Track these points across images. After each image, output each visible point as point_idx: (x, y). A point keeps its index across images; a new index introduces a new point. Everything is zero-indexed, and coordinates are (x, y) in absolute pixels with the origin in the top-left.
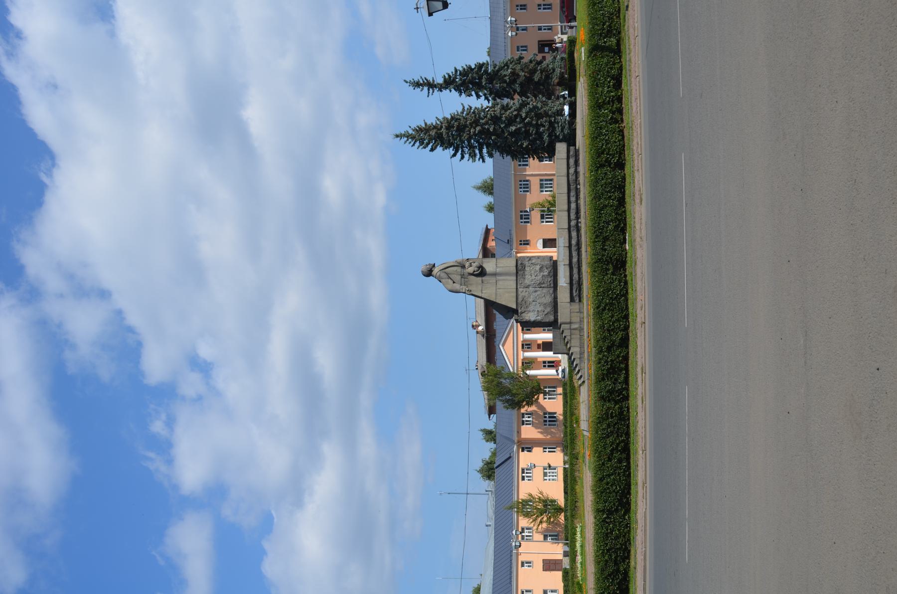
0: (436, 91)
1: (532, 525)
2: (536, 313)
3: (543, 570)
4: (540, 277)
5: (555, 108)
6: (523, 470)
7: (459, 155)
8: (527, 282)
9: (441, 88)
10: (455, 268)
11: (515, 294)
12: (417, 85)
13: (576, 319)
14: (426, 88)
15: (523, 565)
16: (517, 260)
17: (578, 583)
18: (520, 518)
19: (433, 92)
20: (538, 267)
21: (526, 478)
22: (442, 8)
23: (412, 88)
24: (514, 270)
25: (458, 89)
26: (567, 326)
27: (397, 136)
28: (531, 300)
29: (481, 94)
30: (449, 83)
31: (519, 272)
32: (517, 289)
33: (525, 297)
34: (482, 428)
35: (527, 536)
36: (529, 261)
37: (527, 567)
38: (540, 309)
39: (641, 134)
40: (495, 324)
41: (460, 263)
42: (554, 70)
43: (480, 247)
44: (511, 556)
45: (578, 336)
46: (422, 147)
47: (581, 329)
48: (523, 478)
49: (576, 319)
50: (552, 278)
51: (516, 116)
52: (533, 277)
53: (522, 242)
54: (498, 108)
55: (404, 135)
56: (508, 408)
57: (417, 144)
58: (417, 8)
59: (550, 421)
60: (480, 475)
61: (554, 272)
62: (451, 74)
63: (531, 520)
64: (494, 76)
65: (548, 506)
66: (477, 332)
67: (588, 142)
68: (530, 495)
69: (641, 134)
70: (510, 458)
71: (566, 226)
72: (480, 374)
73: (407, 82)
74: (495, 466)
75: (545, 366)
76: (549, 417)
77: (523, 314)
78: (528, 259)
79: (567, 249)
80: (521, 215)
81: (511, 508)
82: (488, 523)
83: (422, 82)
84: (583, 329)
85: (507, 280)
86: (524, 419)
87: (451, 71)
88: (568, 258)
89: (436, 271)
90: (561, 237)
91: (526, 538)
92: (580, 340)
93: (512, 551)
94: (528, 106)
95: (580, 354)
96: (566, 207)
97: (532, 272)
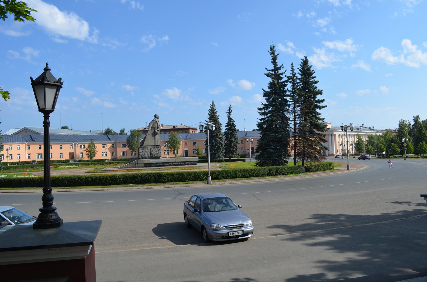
0: (228, 115)
1: (86, 148)
2: (142, 152)
4: (154, 153)
5: (220, 155)
6: (106, 145)
8: (152, 149)
9: (229, 117)
10: (157, 125)
11: (148, 145)
12: (230, 109)
13: (139, 165)
14: (229, 112)
16: (159, 146)
17: (58, 167)
18: (88, 144)
19: (227, 114)
20: (157, 152)
21: (103, 146)
23: (229, 107)
24: (157, 145)
25: (228, 122)
27: (213, 102)
28: (146, 150)
29: (227, 130)
30: (230, 120)
31: (156, 146)
32: (150, 146)
33: (147, 148)
34: (125, 129)
35: (82, 147)
38: (143, 153)
39: (279, 180)
41: (159, 127)
42: (234, 155)
43: (189, 127)
46: (209, 110)
48: (103, 145)
49: (139, 165)
51: (218, 142)
52: (154, 151)
54: (220, 136)
55: (213, 104)
56: (127, 139)
57: (210, 109)
58: (201, 122)
59: (123, 154)
60: (106, 129)
62: (233, 120)
63: (87, 148)
64: (232, 135)
65: (92, 154)
68: (96, 148)
69: (279, 180)
70: (110, 140)
71: (170, 162)
72: (145, 127)
73: (230, 105)
74: (108, 135)
76: (125, 154)
77: (141, 148)
78: (160, 149)
79: (162, 162)
80: (196, 142)
81: (91, 141)
82: (91, 131)
83: (231, 110)
84: (135, 168)
86: (82, 145)
87: (234, 120)
88: (159, 162)
89: (156, 119)
91: (81, 146)
94: (221, 146)
95: (127, 167)
96: (177, 161)
97: (156, 151)
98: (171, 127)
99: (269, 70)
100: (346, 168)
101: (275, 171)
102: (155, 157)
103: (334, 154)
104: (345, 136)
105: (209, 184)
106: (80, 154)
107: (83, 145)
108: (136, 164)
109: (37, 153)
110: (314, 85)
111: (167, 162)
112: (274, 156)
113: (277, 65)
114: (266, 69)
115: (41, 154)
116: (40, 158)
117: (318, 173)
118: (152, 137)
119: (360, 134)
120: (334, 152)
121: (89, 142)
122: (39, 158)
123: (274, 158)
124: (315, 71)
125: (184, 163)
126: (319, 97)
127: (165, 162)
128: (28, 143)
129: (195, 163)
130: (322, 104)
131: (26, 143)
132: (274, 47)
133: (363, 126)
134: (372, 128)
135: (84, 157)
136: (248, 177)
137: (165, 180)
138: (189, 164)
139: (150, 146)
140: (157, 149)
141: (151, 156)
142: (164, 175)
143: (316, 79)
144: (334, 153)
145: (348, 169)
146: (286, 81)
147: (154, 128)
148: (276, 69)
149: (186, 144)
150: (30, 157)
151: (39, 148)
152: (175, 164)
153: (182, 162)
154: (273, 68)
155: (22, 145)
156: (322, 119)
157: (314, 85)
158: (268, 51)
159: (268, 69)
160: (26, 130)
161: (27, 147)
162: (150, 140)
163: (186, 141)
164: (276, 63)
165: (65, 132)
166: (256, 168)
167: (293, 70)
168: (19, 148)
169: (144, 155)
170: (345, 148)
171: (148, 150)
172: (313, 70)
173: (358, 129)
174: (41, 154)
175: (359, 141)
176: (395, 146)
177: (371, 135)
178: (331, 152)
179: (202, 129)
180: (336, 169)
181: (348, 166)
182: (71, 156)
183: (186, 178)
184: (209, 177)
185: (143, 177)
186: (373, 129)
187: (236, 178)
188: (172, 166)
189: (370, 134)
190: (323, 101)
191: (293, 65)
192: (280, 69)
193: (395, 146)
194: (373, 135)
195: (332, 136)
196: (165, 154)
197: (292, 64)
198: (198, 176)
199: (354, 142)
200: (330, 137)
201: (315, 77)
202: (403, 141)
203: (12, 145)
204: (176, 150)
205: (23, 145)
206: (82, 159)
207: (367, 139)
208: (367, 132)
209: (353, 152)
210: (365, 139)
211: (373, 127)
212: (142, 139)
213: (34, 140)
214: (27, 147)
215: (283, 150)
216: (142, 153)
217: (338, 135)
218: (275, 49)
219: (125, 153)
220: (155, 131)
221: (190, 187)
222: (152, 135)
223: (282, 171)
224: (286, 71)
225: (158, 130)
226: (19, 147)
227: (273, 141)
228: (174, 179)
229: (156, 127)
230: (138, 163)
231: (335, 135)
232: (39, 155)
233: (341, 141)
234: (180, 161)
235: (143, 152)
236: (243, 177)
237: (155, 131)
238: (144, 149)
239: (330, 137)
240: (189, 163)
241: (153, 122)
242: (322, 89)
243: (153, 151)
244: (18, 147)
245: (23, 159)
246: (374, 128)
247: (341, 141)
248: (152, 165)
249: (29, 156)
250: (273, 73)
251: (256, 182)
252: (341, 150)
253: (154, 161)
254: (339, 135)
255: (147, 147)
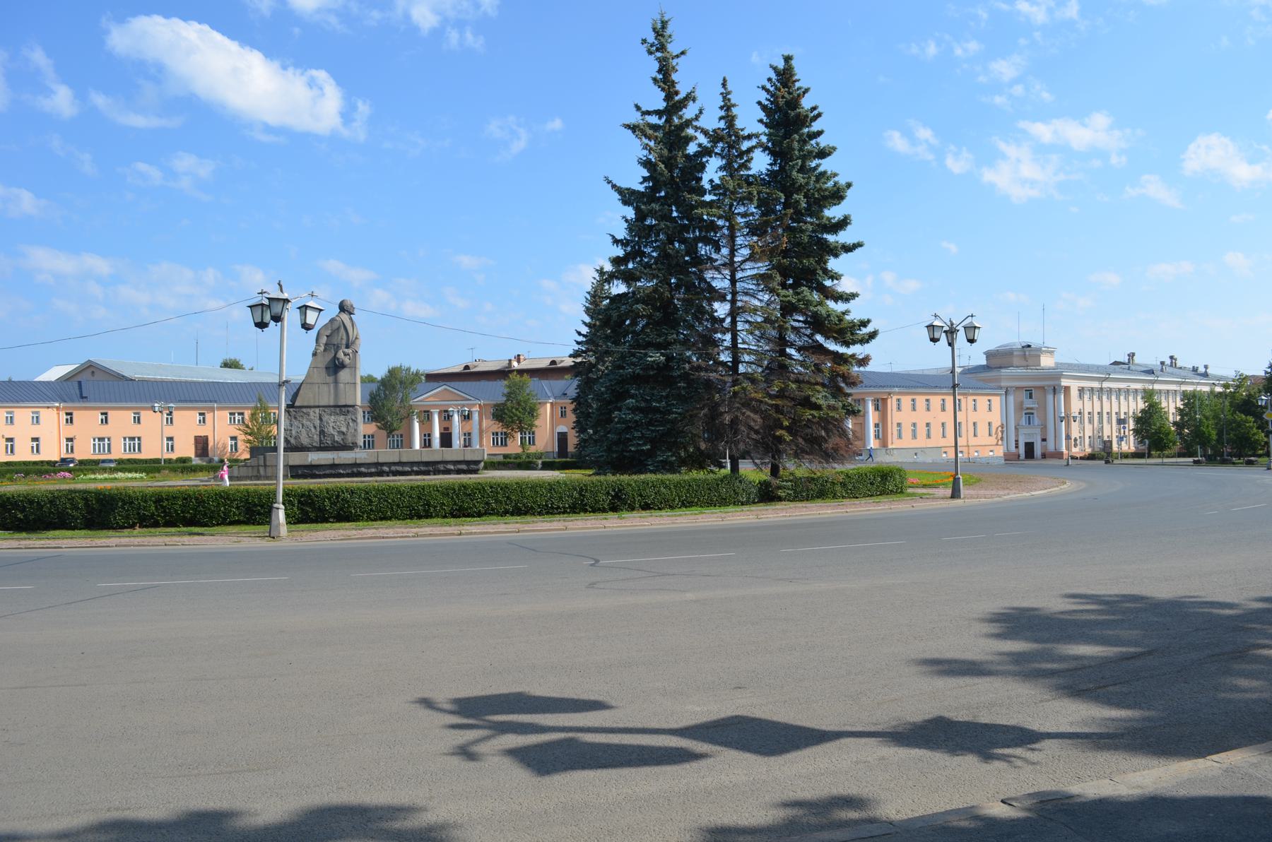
3: (195, 437)
4: (332, 432)
7: (581, 339)
8: (325, 418)
10: (345, 337)
11: (312, 404)
15: (927, 400)
20: (344, 429)
22: (256, 321)
24: (342, 403)
26: (262, 462)
28: (304, 422)
31: (338, 409)
32: (318, 407)
33: (309, 415)
35: (234, 418)
36: (352, 419)
37: (198, 419)
40: (535, 379)
44: (211, 401)
45: (250, 475)
47: (258, 478)
50: (331, 445)
52: (331, 424)
53: (563, 410)
58: (312, 296)
61: (339, 447)
66: (510, 361)
67: (489, 480)
71: (380, 461)
75: (425, 435)
76: (369, 441)
78: (354, 418)
79: (353, 462)
81: (260, 400)
85: (329, 395)
86: (236, 415)
88: (342, 463)
89: (345, 317)
90: (367, 455)
91: (232, 417)
92: (246, 477)
93: (216, 402)
96: (404, 459)
98: (544, 364)
99: (648, 113)
100: (949, 492)
101: (608, 493)
102: (336, 445)
103: (1062, 453)
104: (1102, 394)
105: (274, 538)
106: (230, 442)
107: (239, 414)
108: (259, 466)
109: (94, 436)
110: (818, 166)
111: (416, 463)
112: (640, 438)
113: (677, 93)
114: (638, 108)
115: (106, 440)
116: (134, 450)
117: (854, 504)
118: (328, 377)
119: (1157, 387)
120: (1062, 446)
121: (252, 405)
122: (99, 451)
123: (639, 445)
124: (821, 111)
125: (431, 469)
126: (833, 213)
127: (363, 462)
128: (66, 405)
129: (473, 466)
130: (843, 237)
131: (57, 405)
132: (664, 24)
133: (1172, 363)
134: (1202, 370)
135: (240, 451)
136: (480, 515)
137: (127, 517)
138: (452, 470)
139: (318, 407)
140: (342, 418)
141: (320, 440)
142: (123, 501)
143: (823, 141)
144: (1064, 449)
145: (955, 494)
146: (706, 152)
147: (334, 345)
148: (674, 105)
149: (562, 412)
150: (72, 447)
151: (102, 420)
152: (400, 468)
153: (427, 464)
154: (661, 105)
155: (46, 409)
156: (845, 297)
157: (818, 166)
158: (644, 41)
159: (644, 109)
160: (90, 371)
161: (65, 417)
162: (319, 387)
163: (562, 403)
164: (673, 82)
165: (231, 376)
166: (595, 478)
167: (727, 106)
168: (37, 420)
169: (295, 438)
170: (1100, 434)
171: (310, 420)
172: (764, 88)
173: (1151, 372)
174: (106, 440)
175: (1149, 409)
176: (1247, 425)
177: (1195, 391)
178: (1051, 447)
179: (260, 320)
180: (913, 495)
181: (956, 482)
182: (200, 446)
183: (213, 512)
184: (274, 510)
185: (42, 507)
186: (1206, 372)
187: (428, 516)
188: (388, 476)
189: (1190, 388)
190: (843, 223)
191: (729, 87)
192: (685, 106)
193: (1247, 425)
194: (1201, 391)
195: (1055, 394)
196: (494, 444)
197: (724, 85)
198: (262, 507)
199: (1134, 413)
200: (1050, 397)
201: (819, 133)
202: (1263, 404)
203: (13, 412)
204: (529, 434)
205: (50, 409)
206: (234, 456)
207: (1180, 404)
208: (1182, 383)
209: (1130, 445)
210: (1171, 407)
211: (1206, 367)
212: (77, 366)
213: (86, 397)
214: (64, 417)
215: (676, 413)
216: (291, 430)
217: (1079, 390)
218: (668, 31)
219: (371, 439)
220: (335, 357)
221: (179, 547)
222: (327, 368)
223: (641, 496)
224: (701, 112)
225: (345, 354)
226: (37, 417)
227: (636, 379)
228: (165, 516)
229: (344, 342)
230: (268, 463)
231: (1067, 389)
232: (101, 443)
233: (1088, 409)
234: (416, 460)
235: (291, 426)
236: (518, 511)
237: (337, 356)
238: (295, 418)
239: (1050, 397)
240: (452, 467)
241: (329, 325)
242: (849, 181)
243: (327, 423)
244: (33, 417)
245: (51, 452)
246: (1209, 371)
247: (1088, 409)
248: (317, 473)
249: (70, 443)
250: (661, 122)
251: (475, 533)
252: (1087, 441)
253: (325, 459)
254: (1081, 390)
255: (308, 410)
